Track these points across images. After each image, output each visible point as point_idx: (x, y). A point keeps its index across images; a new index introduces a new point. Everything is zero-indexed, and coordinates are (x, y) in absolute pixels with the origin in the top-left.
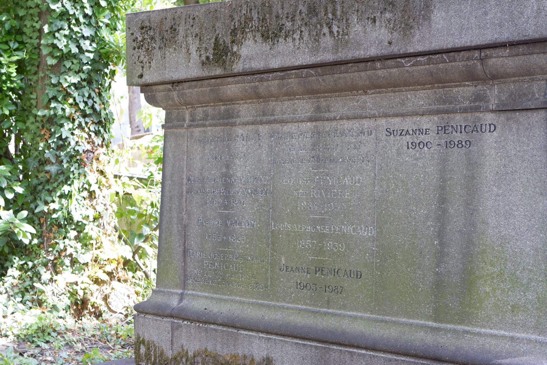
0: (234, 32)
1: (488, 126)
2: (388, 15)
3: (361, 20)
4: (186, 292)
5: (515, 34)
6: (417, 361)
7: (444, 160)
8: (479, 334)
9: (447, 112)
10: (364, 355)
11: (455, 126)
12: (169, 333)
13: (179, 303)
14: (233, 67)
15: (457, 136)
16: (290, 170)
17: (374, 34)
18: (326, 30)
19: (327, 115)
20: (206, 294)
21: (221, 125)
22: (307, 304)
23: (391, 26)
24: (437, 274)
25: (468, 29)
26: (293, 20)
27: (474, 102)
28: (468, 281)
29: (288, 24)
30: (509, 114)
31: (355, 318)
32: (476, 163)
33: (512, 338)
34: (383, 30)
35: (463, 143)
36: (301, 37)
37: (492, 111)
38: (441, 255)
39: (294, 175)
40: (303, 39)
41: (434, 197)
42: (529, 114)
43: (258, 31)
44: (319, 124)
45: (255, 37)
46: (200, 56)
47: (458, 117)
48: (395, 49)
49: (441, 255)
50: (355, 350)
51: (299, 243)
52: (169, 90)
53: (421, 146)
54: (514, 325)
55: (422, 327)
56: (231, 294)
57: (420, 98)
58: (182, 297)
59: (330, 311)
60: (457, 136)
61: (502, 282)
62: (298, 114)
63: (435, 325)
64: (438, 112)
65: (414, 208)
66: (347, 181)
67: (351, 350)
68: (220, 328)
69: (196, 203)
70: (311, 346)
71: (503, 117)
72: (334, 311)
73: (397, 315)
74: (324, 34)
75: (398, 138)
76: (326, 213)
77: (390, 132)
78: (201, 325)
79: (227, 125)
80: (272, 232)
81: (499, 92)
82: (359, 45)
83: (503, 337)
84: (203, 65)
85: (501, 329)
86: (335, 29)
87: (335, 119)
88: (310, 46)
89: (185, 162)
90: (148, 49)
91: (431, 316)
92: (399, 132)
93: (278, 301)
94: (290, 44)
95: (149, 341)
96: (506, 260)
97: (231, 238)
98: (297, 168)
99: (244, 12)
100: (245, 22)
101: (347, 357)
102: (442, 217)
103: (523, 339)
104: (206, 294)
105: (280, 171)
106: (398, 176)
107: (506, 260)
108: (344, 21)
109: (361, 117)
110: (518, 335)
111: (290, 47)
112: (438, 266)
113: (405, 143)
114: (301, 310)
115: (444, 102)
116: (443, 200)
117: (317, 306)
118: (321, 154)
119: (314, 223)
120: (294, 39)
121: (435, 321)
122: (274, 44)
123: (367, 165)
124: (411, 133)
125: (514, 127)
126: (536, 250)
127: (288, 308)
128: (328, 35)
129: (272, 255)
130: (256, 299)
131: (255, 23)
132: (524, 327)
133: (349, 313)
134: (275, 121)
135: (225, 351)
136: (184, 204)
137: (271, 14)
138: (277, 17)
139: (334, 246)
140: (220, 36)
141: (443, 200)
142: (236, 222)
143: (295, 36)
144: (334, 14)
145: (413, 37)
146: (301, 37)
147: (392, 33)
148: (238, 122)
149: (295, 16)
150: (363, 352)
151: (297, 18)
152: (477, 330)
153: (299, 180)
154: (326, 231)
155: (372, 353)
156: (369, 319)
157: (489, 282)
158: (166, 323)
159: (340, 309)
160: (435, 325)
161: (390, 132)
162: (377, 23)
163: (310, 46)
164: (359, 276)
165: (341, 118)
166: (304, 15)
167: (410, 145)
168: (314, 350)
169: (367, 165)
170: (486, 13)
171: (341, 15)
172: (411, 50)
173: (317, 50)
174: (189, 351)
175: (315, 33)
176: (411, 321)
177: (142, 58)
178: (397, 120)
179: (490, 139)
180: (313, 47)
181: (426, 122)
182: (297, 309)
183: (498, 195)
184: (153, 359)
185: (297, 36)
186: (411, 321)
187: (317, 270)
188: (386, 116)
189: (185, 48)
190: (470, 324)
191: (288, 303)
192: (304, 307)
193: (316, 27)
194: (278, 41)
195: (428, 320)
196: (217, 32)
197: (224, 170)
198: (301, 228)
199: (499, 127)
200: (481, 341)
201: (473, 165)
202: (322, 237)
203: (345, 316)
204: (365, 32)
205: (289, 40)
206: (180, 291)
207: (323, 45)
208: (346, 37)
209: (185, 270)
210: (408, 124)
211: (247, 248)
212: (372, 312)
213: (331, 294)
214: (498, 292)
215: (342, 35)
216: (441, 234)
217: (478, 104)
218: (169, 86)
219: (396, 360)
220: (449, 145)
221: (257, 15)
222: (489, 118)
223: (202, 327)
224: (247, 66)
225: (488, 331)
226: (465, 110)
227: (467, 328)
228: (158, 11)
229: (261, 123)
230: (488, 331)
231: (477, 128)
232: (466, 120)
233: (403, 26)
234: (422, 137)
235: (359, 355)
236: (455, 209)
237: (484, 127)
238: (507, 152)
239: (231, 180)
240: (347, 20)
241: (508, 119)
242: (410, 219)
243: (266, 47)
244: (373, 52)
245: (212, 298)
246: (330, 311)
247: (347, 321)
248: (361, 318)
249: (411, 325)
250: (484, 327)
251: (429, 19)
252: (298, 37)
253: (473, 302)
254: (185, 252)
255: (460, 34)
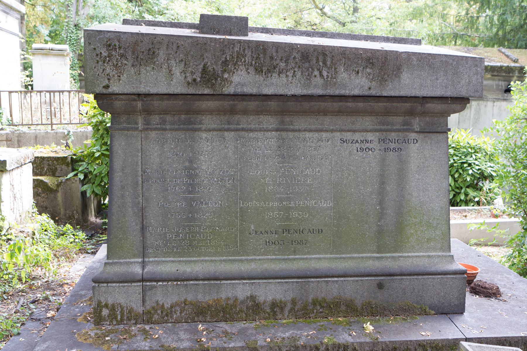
0: (225, 63)
1: (412, 140)
2: (368, 70)
3: (347, 70)
4: (146, 260)
5: (455, 93)
6: (376, 278)
7: (383, 160)
8: (409, 257)
9: (387, 131)
10: (337, 281)
11: (391, 139)
12: (139, 294)
13: (143, 269)
14: (224, 89)
15: (392, 145)
16: (257, 164)
17: (357, 81)
18: (316, 73)
19: (292, 127)
20: (172, 259)
21: (183, 130)
22: (276, 255)
23: (371, 77)
24: (379, 225)
25: (425, 87)
26: (287, 62)
27: (404, 126)
28: (400, 227)
29: (283, 65)
30: (426, 134)
31: (320, 259)
32: (405, 161)
33: (429, 256)
34: (364, 79)
35: (397, 149)
36: (294, 75)
37: (417, 132)
38: (381, 215)
39: (260, 167)
40: (295, 76)
41: (377, 181)
42: (438, 134)
43: (251, 65)
44: (284, 134)
45: (248, 69)
46: (186, 77)
47: (393, 134)
48: (373, 92)
49: (381, 215)
50: (329, 279)
51: (268, 215)
52: (134, 100)
53: (367, 150)
54: (428, 249)
55: (370, 258)
56: (199, 256)
57: (367, 122)
58: (143, 265)
59: (297, 257)
60: (392, 145)
61: (422, 227)
62: (263, 125)
63: (378, 255)
64: (381, 130)
65: (362, 188)
66: (308, 172)
67: (326, 279)
68: (201, 282)
69: (155, 190)
70: (292, 282)
71: (422, 136)
72: (300, 256)
73: (350, 253)
74: (315, 76)
75: (350, 144)
76: (291, 193)
77: (343, 141)
78: (179, 283)
79: (188, 130)
80: (241, 208)
81: (420, 121)
82: (345, 86)
83: (423, 256)
84: (188, 85)
85: (421, 252)
86: (325, 73)
87: (299, 131)
88: (302, 82)
89: (140, 158)
90: (117, 64)
91: (375, 250)
92: (351, 141)
93: (248, 256)
94: (284, 79)
95: (113, 304)
96: (424, 215)
97: (197, 214)
98: (264, 163)
99: (236, 49)
100: (238, 57)
101: (324, 285)
102: (382, 193)
103: (435, 256)
104: (172, 259)
105: (247, 165)
106: (350, 169)
107: (424, 215)
108: (333, 69)
109: (321, 131)
110: (431, 254)
111: (283, 81)
112: (379, 221)
113: (355, 148)
114: (272, 259)
115: (384, 125)
116: (383, 183)
117: (285, 255)
118: (285, 154)
119: (281, 200)
120: (287, 76)
121: (378, 253)
122: (267, 77)
123: (325, 162)
124: (360, 142)
125: (429, 142)
126: (441, 208)
127: (259, 260)
128: (318, 76)
129: (241, 224)
130: (226, 256)
131: (248, 59)
132: (435, 249)
133: (313, 256)
134: (243, 130)
135: (207, 298)
136: (141, 191)
137: (265, 54)
138: (272, 58)
139: (299, 214)
140: (209, 64)
141: (383, 183)
142: (203, 203)
143: (288, 73)
144: (324, 63)
145: (387, 86)
146: (294, 75)
147: (371, 82)
148: (203, 128)
149: (288, 59)
150: (336, 279)
151: (291, 61)
152: (406, 254)
153: (265, 171)
154: (292, 205)
155: (342, 279)
156: (330, 258)
157: (413, 227)
158: (137, 287)
159: (305, 254)
160: (378, 255)
161: (343, 141)
162: (360, 74)
163: (302, 82)
164: (320, 231)
165: (305, 131)
166: (297, 60)
167: (359, 150)
168: (295, 284)
169: (325, 162)
170: (437, 79)
171: (330, 65)
172: (385, 94)
173: (309, 87)
174: (165, 304)
175: (307, 74)
176: (361, 255)
177: (108, 71)
178: (349, 134)
179: (414, 148)
180: (305, 83)
181: (370, 136)
182: (268, 259)
183: (419, 179)
184: (119, 317)
185: (290, 74)
186: (361, 255)
187: (285, 231)
188: (341, 131)
189: (166, 69)
190: (401, 251)
191: (259, 256)
192: (274, 257)
193: (308, 70)
194: (271, 76)
195: (373, 253)
196: (206, 60)
197: (187, 164)
198: (268, 204)
199: (419, 141)
200: (410, 260)
201: (403, 163)
202: (288, 209)
203: (311, 259)
204: (350, 79)
205: (283, 76)
206: (140, 260)
207: (314, 83)
208: (334, 80)
209: (144, 242)
210: (358, 136)
211: (215, 221)
212: (331, 254)
213: (297, 246)
214: (419, 232)
215: (331, 78)
216: (381, 202)
217: (407, 128)
218: (136, 97)
219: (361, 280)
220: (386, 150)
221: (250, 53)
222: (413, 135)
223: (180, 284)
224: (239, 90)
225: (413, 254)
226: (399, 131)
227: (401, 254)
228: (132, 33)
229: (228, 130)
230: (413, 254)
231: (406, 141)
232: (398, 136)
233: (380, 78)
234: (367, 145)
235: (333, 281)
236: (391, 187)
237: (410, 141)
238: (425, 155)
239: (195, 172)
240: (335, 69)
241: (425, 137)
242: (359, 195)
243: (260, 78)
244: (356, 92)
245: (180, 261)
246: (297, 257)
247: (313, 261)
248: (324, 258)
249: (363, 257)
250: (410, 252)
251: (399, 77)
252: (292, 74)
253: (403, 239)
254: (143, 229)
255: (420, 89)
